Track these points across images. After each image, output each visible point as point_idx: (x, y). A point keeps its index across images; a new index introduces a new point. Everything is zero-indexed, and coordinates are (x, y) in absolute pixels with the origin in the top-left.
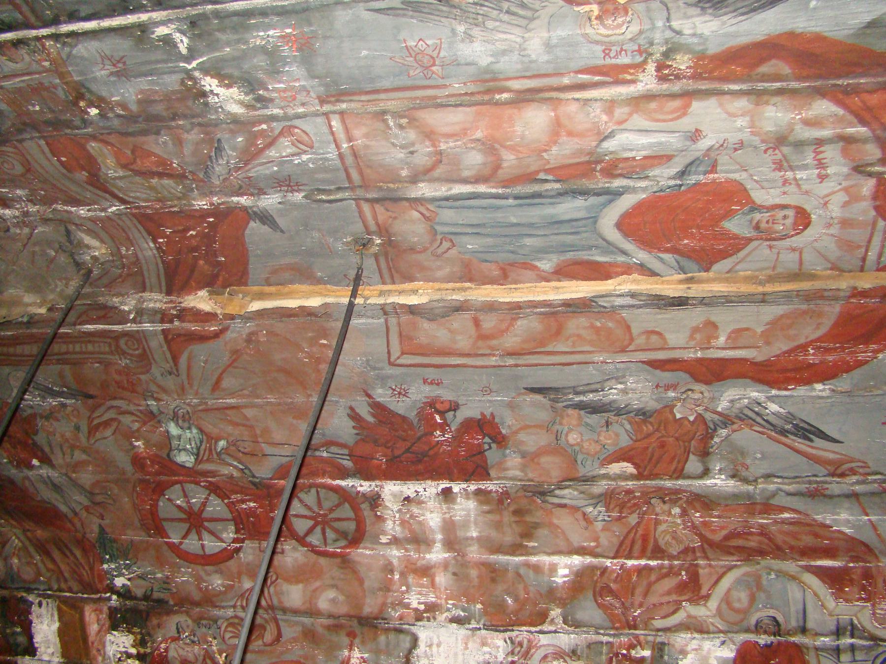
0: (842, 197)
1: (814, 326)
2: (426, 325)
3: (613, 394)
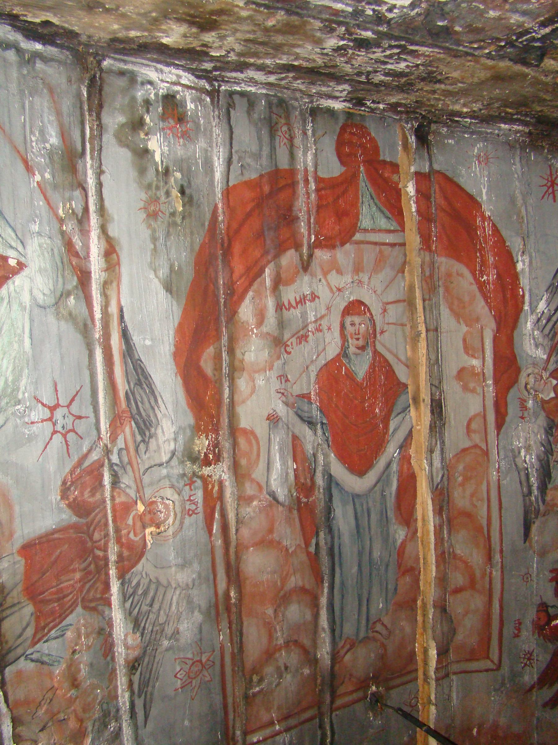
0: (334, 279)
1: (460, 278)
2: (460, 637)
3: (530, 459)
